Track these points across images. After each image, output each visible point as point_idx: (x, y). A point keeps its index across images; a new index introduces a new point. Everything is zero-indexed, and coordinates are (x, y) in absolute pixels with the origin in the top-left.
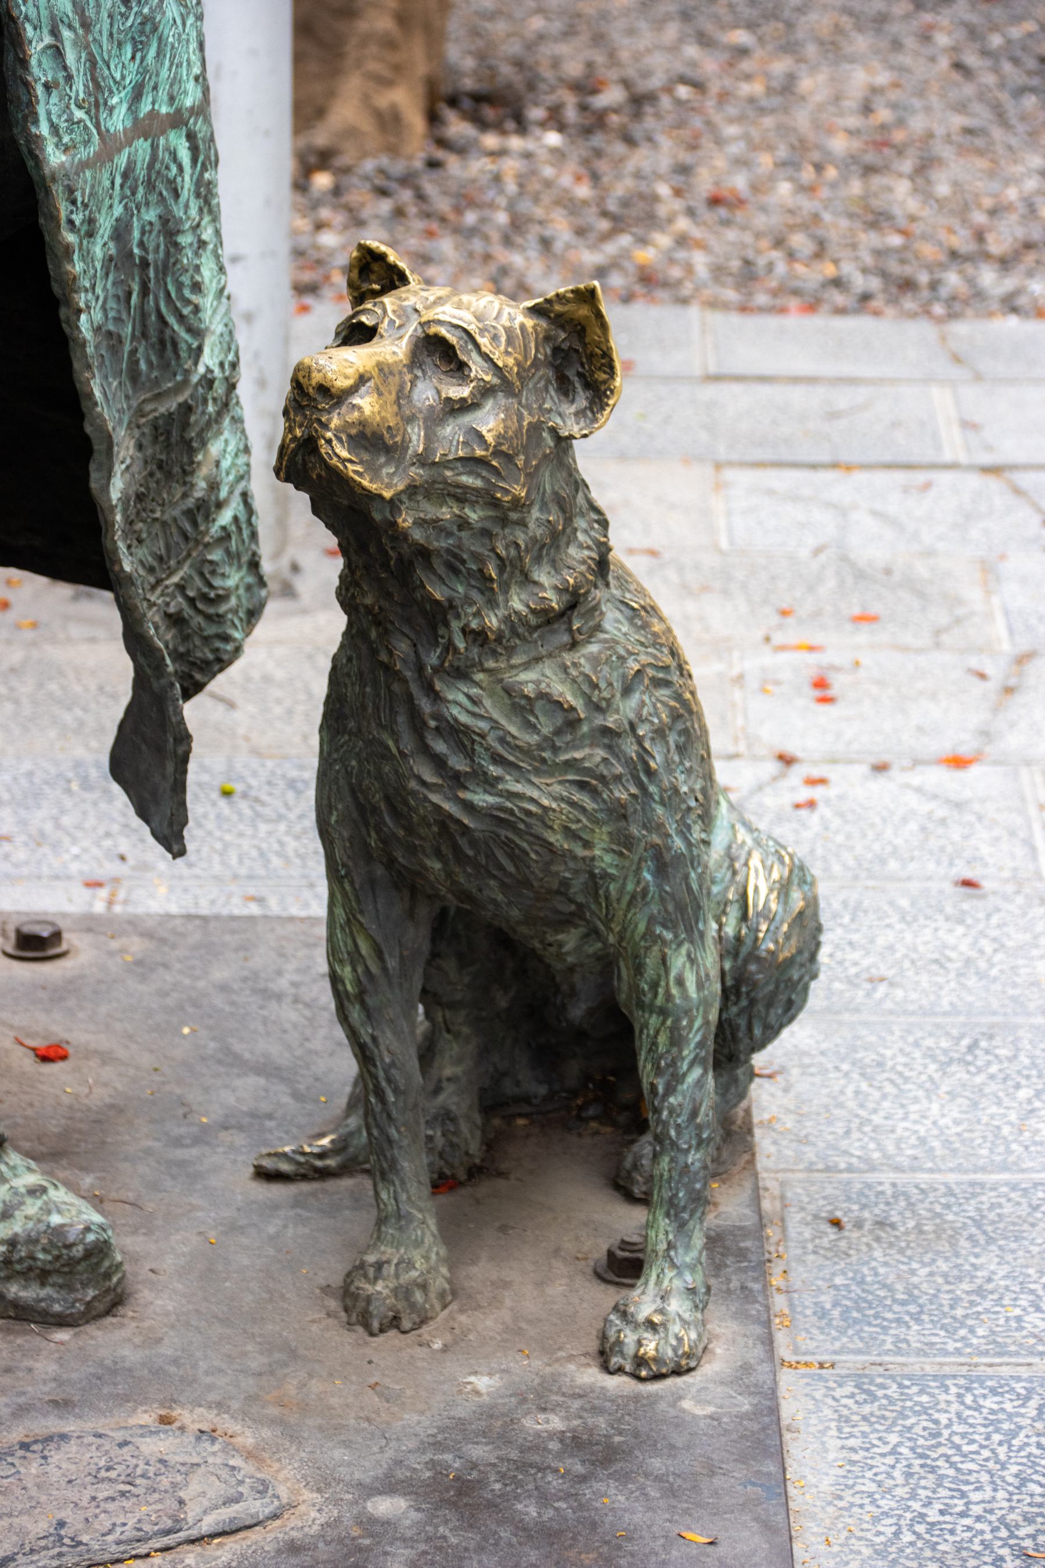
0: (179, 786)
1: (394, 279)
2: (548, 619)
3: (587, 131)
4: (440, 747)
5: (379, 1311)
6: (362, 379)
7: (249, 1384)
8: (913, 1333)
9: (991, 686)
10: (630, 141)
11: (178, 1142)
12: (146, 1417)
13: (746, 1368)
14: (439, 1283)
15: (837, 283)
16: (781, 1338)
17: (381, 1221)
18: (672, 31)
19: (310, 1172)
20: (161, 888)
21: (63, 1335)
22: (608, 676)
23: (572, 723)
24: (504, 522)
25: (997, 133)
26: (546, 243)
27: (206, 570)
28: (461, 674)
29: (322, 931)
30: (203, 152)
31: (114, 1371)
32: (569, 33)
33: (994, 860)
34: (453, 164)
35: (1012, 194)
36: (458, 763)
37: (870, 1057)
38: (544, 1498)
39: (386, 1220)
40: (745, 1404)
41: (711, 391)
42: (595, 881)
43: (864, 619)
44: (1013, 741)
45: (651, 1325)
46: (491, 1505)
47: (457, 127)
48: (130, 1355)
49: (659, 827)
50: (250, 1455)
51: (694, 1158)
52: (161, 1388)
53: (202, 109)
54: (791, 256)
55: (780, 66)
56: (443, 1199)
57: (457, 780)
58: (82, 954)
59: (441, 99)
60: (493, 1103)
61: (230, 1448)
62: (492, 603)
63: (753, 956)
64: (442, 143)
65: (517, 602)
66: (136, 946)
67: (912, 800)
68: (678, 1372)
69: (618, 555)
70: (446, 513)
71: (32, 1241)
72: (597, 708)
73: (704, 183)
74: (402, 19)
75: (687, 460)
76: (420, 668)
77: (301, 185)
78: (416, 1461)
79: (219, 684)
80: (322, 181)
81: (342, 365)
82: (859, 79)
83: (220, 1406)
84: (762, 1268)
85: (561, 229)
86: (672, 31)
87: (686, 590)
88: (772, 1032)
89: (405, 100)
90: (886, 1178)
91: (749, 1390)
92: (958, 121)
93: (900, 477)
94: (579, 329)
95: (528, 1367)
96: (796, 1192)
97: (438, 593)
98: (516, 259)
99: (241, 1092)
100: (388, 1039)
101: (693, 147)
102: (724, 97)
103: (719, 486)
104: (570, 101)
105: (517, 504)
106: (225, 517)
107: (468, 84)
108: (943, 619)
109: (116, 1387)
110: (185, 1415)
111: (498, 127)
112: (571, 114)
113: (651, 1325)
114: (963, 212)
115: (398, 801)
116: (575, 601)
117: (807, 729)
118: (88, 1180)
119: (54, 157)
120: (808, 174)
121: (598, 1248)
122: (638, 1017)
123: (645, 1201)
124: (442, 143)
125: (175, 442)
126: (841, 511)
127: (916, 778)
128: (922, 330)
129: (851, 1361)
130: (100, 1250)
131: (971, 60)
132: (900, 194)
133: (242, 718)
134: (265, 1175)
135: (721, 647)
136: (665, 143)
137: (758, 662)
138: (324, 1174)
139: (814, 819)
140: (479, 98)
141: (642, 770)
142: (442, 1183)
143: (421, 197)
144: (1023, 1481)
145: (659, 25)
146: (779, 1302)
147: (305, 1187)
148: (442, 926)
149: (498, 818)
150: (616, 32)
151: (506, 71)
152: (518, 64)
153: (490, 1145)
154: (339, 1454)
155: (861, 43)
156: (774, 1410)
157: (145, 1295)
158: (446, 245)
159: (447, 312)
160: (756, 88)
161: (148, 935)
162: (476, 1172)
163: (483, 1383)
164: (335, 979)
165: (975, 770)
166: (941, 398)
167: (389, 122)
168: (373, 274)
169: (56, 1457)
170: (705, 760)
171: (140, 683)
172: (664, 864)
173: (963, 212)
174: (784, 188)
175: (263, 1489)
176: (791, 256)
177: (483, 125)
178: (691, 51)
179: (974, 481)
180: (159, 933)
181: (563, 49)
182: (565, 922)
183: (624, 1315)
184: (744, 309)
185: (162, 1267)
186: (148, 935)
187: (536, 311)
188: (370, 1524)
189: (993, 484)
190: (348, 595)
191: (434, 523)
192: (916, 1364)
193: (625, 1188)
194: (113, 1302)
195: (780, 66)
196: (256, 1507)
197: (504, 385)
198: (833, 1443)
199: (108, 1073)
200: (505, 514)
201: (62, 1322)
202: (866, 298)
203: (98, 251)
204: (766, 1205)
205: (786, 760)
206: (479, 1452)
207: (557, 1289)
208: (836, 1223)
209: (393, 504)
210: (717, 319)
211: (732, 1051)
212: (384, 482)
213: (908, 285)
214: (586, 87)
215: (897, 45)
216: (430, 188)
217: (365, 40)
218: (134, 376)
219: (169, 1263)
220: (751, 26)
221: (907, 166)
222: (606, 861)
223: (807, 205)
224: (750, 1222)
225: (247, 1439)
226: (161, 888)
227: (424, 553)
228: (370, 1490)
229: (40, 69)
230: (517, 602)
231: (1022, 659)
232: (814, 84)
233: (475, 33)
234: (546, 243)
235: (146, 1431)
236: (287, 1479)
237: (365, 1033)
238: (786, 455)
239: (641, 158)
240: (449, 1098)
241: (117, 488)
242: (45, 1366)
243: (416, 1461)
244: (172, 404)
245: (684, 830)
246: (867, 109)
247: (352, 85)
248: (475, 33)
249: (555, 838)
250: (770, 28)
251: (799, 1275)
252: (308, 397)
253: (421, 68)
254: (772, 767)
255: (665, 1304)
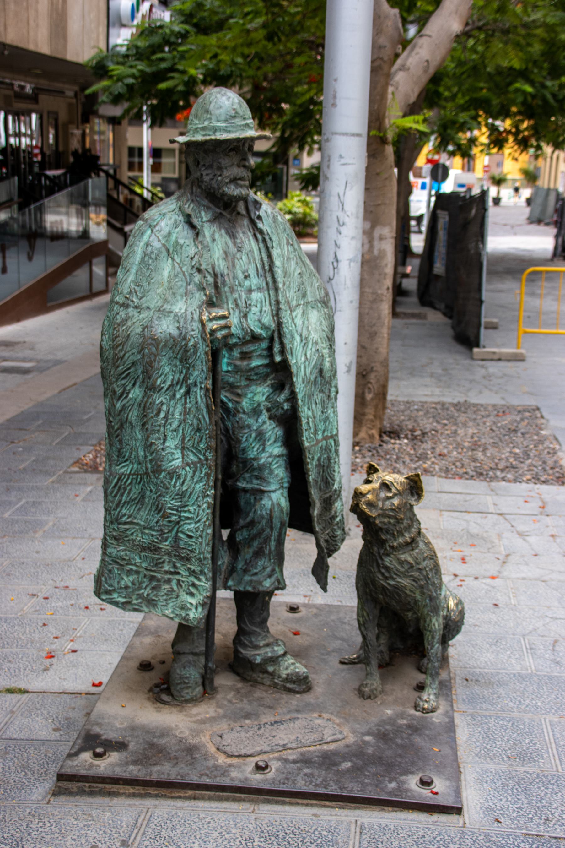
0: (326, 577)
1: (376, 470)
2: (407, 544)
3: (413, 440)
4: (383, 571)
5: (366, 694)
6: (369, 491)
7: (338, 709)
8: (484, 706)
9: (500, 561)
10: (422, 442)
11: (323, 654)
12: (316, 715)
13: (447, 712)
14: (379, 689)
15: (466, 473)
16: (455, 705)
17: (367, 674)
18: (431, 420)
19: (351, 662)
20: (320, 598)
21: (298, 696)
22: (420, 557)
23: (412, 567)
24: (398, 522)
25: (500, 444)
26: (404, 462)
27: (333, 530)
28: (388, 555)
29: (356, 609)
30: (337, 443)
31: (308, 704)
32: (409, 420)
33: (501, 600)
34: (385, 445)
35: (503, 456)
36: (387, 574)
37: (474, 643)
38: (402, 739)
39: (368, 674)
40: (447, 720)
41: (439, 495)
42: (416, 602)
43: (473, 545)
44: (505, 574)
45: (426, 701)
46: (391, 739)
47: (386, 438)
48: (312, 701)
49: (430, 591)
50: (338, 725)
51: (436, 664)
52: (319, 708)
53: (337, 435)
54: (456, 467)
55: (454, 428)
56: (381, 670)
57: (386, 578)
58: (303, 612)
59: (382, 432)
60: (392, 649)
61: (334, 723)
62: (395, 540)
63: (450, 620)
64: (382, 441)
65: (401, 540)
66: (315, 610)
67: (483, 586)
68: (432, 712)
69: (423, 531)
70: (386, 520)
71: (292, 675)
72: (418, 564)
73: (438, 451)
74: (375, 416)
75: (434, 509)
76: (379, 553)
77: (353, 450)
78: (374, 729)
79: (335, 555)
80: (357, 448)
81: (364, 488)
82: (470, 431)
83: (332, 714)
84: (450, 689)
85: (407, 459)
86: (431, 420)
87: (434, 537)
88: (453, 637)
89: (375, 432)
90: (478, 670)
91: (448, 717)
92: (492, 441)
93: (480, 515)
94: (416, 482)
95: (399, 709)
96: (458, 672)
97: (383, 537)
98: (398, 466)
99: (337, 644)
100: (370, 634)
101: (435, 444)
102: (442, 434)
103: (441, 515)
104: (409, 433)
105: (401, 519)
106: (338, 519)
107: (388, 429)
108: (490, 546)
109: (309, 708)
110: (324, 715)
111: (394, 438)
112: (409, 436)
113: (426, 701)
114: (493, 459)
115: (374, 582)
116: (413, 540)
117: (460, 569)
118: (304, 662)
119: (306, 444)
120: (460, 450)
121: (415, 683)
122: (425, 632)
123: (425, 673)
124: (382, 441)
125: (328, 503)
126: (467, 521)
127: (484, 581)
128: (484, 484)
129: (470, 711)
130: (306, 678)
131: (494, 428)
132: (480, 455)
133: (338, 561)
134: (342, 663)
135: (442, 550)
136: (429, 442)
137: (449, 554)
138: (354, 663)
139: (462, 589)
140: (390, 432)
141: (427, 578)
142: (380, 666)
143: (378, 452)
144: (508, 740)
145: (428, 418)
146: (454, 697)
147: (350, 666)
148: (382, 610)
149: (395, 587)
150: (419, 420)
151: (396, 427)
152: (399, 426)
153: (391, 658)
154: (358, 726)
155: (471, 424)
156: (453, 722)
157: (316, 688)
158: (383, 462)
159: (388, 478)
160: (449, 432)
161: (317, 608)
162: (388, 665)
163: (389, 712)
164: (358, 621)
165: (497, 580)
166: (489, 498)
167: (371, 437)
168: (372, 470)
169: (297, 722)
170: (440, 576)
171: (319, 554)
172: (431, 598)
173: (493, 459)
174: (455, 453)
175: (341, 732)
176: (456, 467)
177: (391, 438)
178: (435, 424)
179: (496, 517)
180: (320, 608)
181: (408, 423)
182: (409, 610)
183: (420, 698)
184: (446, 478)
185: (319, 682)
186: (317, 608)
187: (407, 478)
188: (364, 742)
189: (500, 517)
190: (364, 537)
191: (384, 523)
192: (485, 713)
193: (420, 669)
194: (309, 689)
195: (454, 428)
196: (340, 736)
197: (399, 493)
198: (466, 729)
199: (308, 638)
200: (399, 521)
201: (298, 693)
202: (472, 476)
203: (314, 463)
204: (452, 675)
205: (456, 576)
206: (388, 727)
207: (405, 692)
208: (467, 680)
209: (375, 518)
210: (440, 479)
211: (445, 641)
212: (373, 513)
213: (481, 474)
214: (413, 431)
215: (478, 425)
216: (380, 450)
217: (367, 420)
218: (320, 489)
219: (321, 681)
220: (448, 420)
221: (481, 449)
222: (418, 597)
223: (460, 456)
224: (448, 679)
225: (337, 721)
226: (320, 598)
227: (381, 529)
228: (364, 734)
229: (304, 426)
230: (401, 540)
231: (507, 556)
232: (461, 432)
233: (389, 419)
234: (404, 462)
235: (316, 718)
236: (346, 731)
237: (365, 633)
238: (455, 509)
239: (424, 446)
240: (382, 648)
241: (316, 513)
242: (294, 702)
243: (374, 729)
244: (328, 495)
245: (436, 591)
246: (472, 437)
247: (364, 429)
248: (389, 419)
249: (408, 592)
250: (451, 420)
251: (459, 691)
252: (358, 495)
253: (379, 426)
254: (453, 577)
255: (429, 697)
